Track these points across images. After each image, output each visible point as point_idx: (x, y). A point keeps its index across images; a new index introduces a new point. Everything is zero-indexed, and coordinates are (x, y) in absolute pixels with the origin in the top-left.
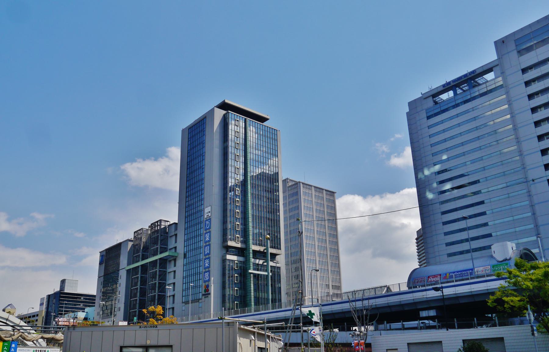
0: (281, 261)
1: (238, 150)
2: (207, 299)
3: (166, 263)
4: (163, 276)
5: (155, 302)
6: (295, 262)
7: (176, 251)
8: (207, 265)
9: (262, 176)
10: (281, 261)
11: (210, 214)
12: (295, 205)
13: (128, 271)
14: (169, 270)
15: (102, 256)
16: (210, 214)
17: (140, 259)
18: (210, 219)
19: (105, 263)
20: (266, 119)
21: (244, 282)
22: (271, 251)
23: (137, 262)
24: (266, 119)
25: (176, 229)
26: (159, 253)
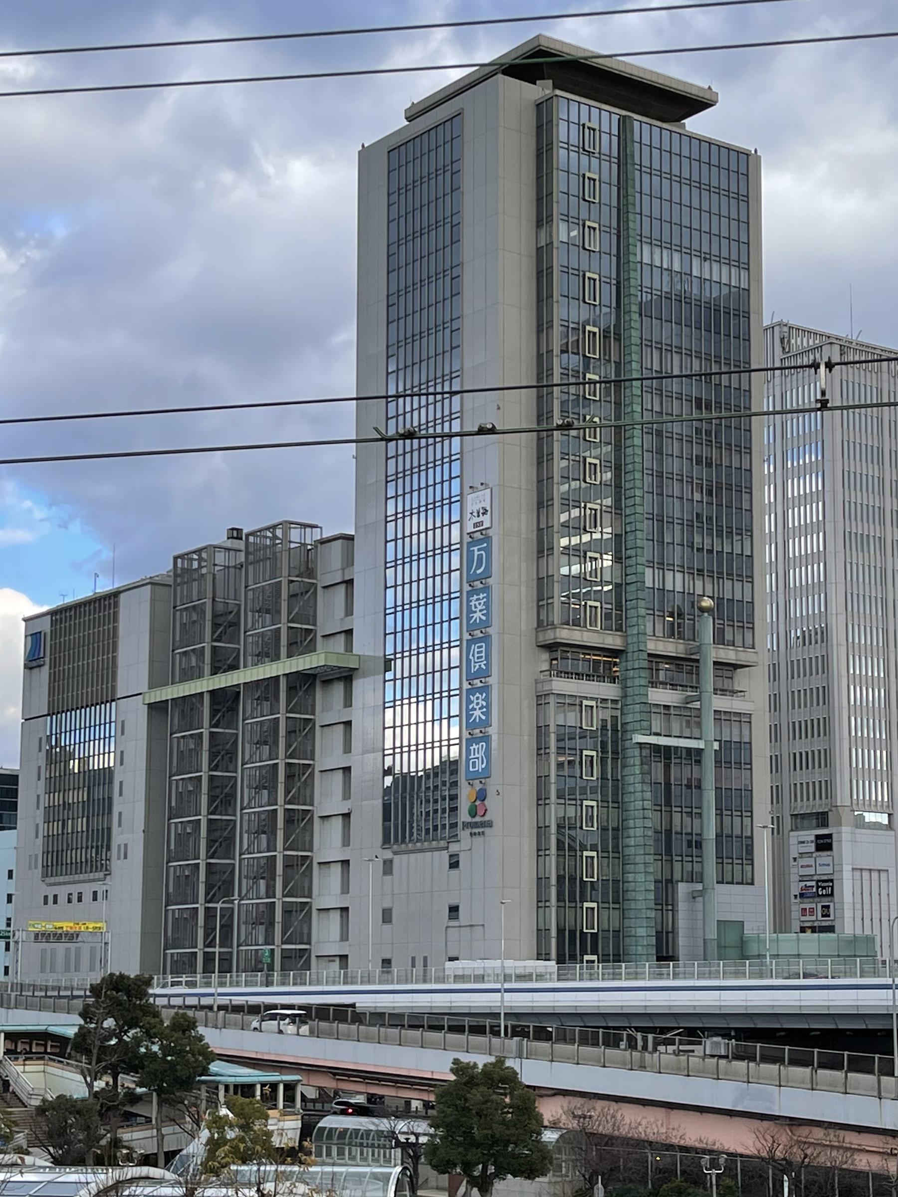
0: (753, 695)
1: (595, 257)
2: (477, 839)
3: (312, 686)
4: (302, 732)
5: (276, 743)
6: (799, 730)
7: (349, 646)
8: (477, 713)
9: (679, 304)
10: (753, 695)
11: (486, 520)
12: (817, 682)
13: (157, 709)
14: (321, 718)
15: (35, 639)
16: (486, 520)
17: (207, 669)
18: (488, 539)
19: (54, 664)
20: (694, 104)
21: (615, 742)
22: (715, 653)
23: (189, 675)
24: (694, 104)
25: (349, 560)
26: (283, 651)
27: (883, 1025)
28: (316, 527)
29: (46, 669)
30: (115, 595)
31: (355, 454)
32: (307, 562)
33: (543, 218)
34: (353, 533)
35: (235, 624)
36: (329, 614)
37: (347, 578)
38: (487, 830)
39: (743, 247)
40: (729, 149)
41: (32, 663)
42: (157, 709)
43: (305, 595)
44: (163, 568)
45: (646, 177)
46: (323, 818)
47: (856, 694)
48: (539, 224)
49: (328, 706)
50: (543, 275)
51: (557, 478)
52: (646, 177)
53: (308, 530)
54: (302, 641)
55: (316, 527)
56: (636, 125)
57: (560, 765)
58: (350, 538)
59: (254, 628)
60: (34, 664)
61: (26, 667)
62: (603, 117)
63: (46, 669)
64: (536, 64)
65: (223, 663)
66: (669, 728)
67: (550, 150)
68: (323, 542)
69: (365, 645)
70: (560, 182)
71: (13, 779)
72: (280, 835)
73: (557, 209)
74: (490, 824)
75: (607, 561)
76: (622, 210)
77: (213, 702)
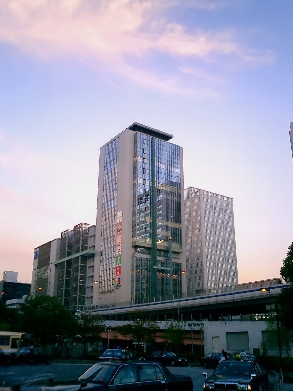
2: (118, 289)
3: (87, 258)
4: (84, 270)
7: (94, 249)
23: (64, 257)
25: (95, 231)
26: (80, 251)
27: (205, 280)
28: (89, 224)
29: (37, 259)
30: (50, 242)
31: (102, 146)
32: (86, 232)
33: (135, 155)
34: (96, 225)
35: (72, 247)
36: (90, 243)
37: (94, 234)
38: (120, 287)
39: (179, 165)
40: (175, 145)
41: (35, 258)
42: (57, 265)
43: (85, 241)
44: (59, 236)
45: (157, 150)
46: (87, 298)
47: (209, 271)
48: (134, 157)
49: (89, 264)
50: (135, 168)
51: (136, 225)
52: (157, 163)
53: (87, 225)
54: (84, 248)
55: (89, 224)
56: (155, 139)
57: (136, 272)
58: (95, 226)
59: (75, 247)
60: (35, 258)
61: (34, 259)
62: (149, 137)
63: (37, 259)
64: (135, 127)
65: (69, 254)
66: (160, 254)
67: (136, 143)
68: (90, 227)
69: (98, 249)
70: (139, 149)
71: (29, 285)
72: (78, 302)
73: (139, 154)
74: (120, 286)
75: (148, 218)
76: (153, 155)
77: (67, 262)
